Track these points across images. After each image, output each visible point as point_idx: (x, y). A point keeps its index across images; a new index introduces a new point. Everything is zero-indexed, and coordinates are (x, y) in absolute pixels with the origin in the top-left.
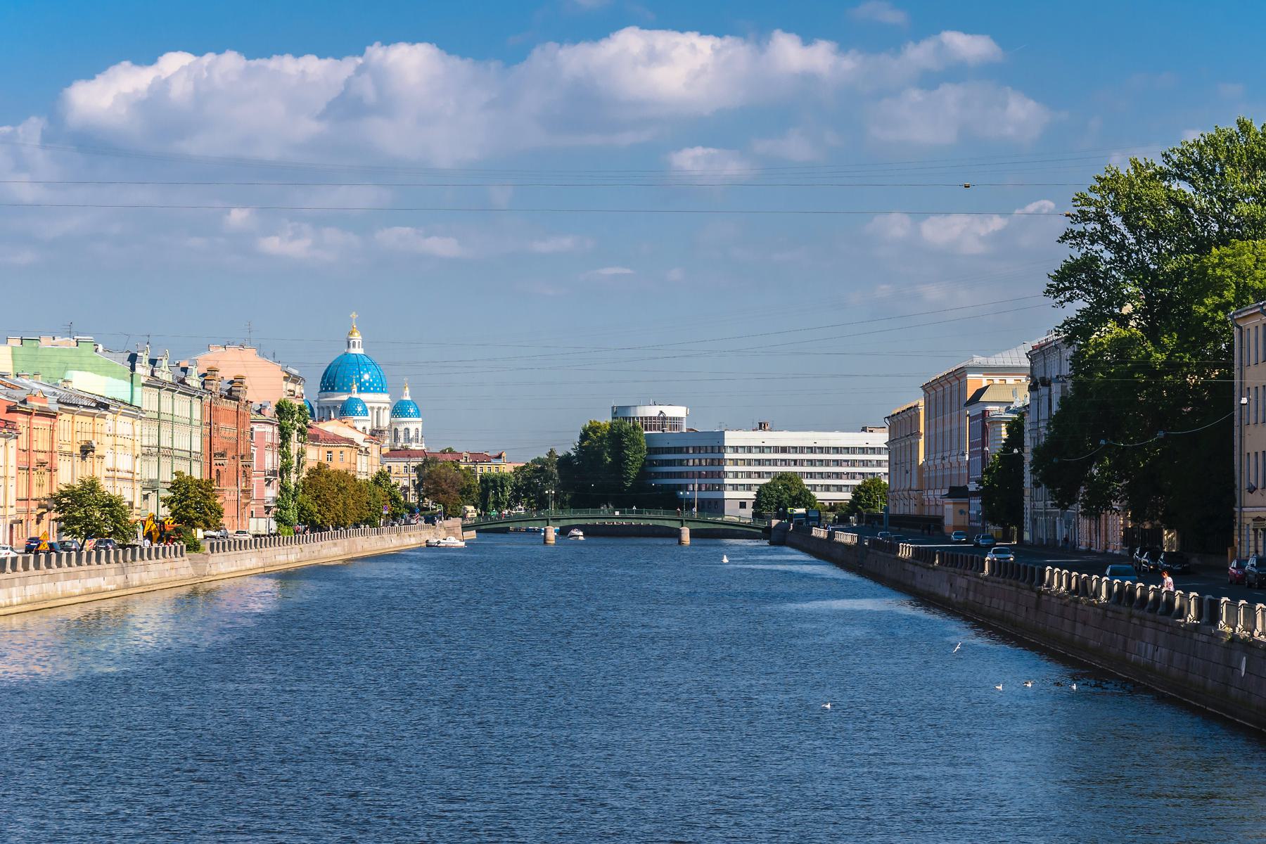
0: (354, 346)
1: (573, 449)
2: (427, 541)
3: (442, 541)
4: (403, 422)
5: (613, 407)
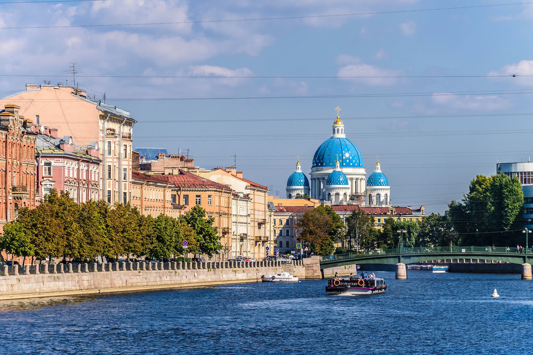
0: (338, 132)
1: (463, 200)
2: (263, 277)
3: (276, 276)
4: (375, 190)
5: (497, 164)
